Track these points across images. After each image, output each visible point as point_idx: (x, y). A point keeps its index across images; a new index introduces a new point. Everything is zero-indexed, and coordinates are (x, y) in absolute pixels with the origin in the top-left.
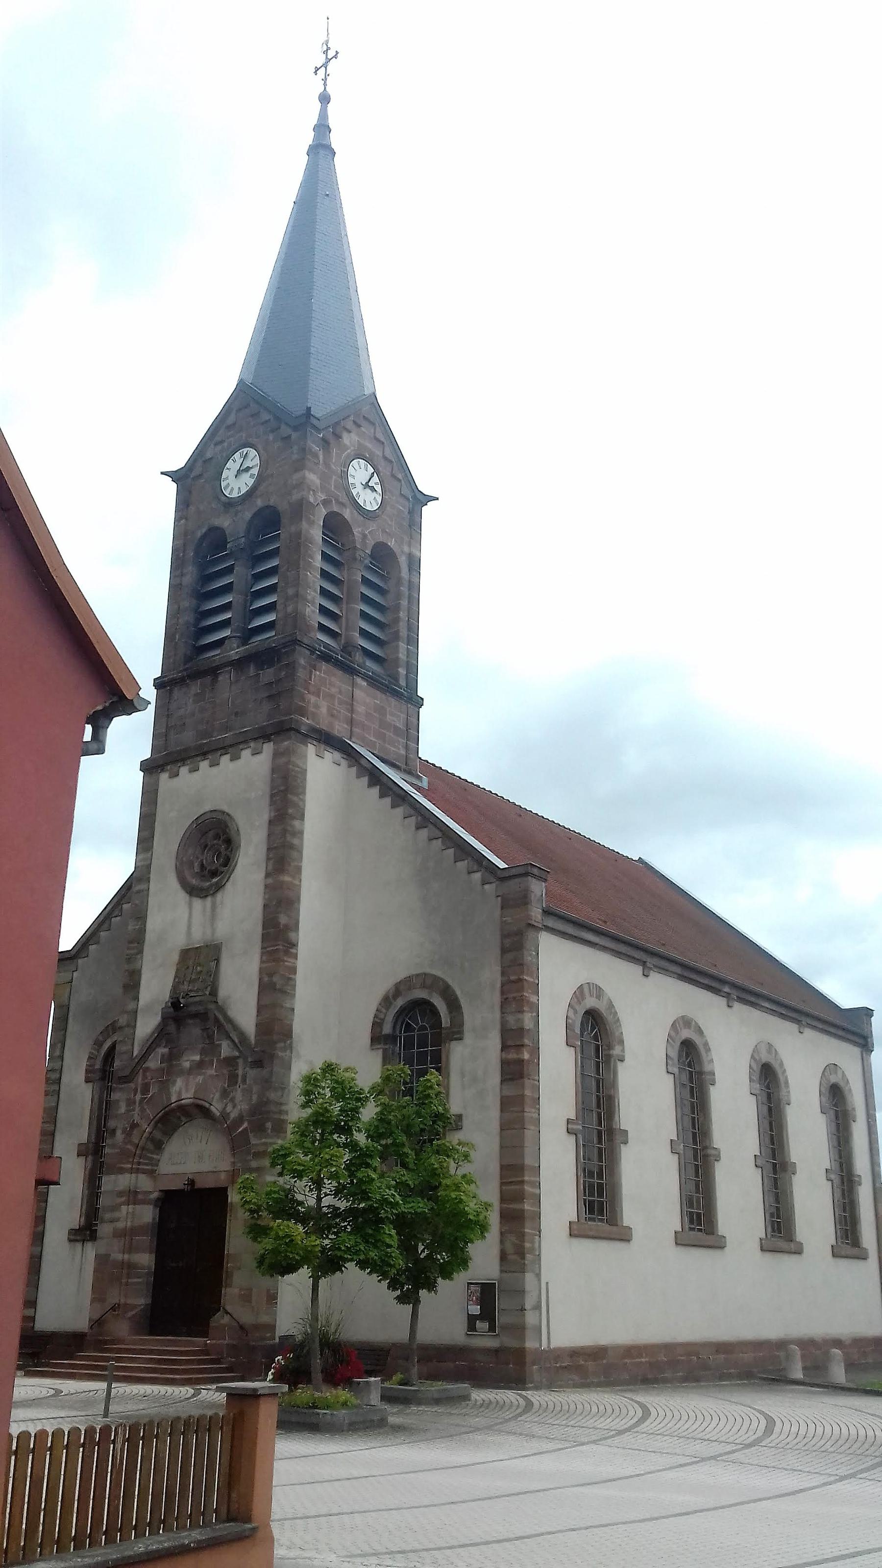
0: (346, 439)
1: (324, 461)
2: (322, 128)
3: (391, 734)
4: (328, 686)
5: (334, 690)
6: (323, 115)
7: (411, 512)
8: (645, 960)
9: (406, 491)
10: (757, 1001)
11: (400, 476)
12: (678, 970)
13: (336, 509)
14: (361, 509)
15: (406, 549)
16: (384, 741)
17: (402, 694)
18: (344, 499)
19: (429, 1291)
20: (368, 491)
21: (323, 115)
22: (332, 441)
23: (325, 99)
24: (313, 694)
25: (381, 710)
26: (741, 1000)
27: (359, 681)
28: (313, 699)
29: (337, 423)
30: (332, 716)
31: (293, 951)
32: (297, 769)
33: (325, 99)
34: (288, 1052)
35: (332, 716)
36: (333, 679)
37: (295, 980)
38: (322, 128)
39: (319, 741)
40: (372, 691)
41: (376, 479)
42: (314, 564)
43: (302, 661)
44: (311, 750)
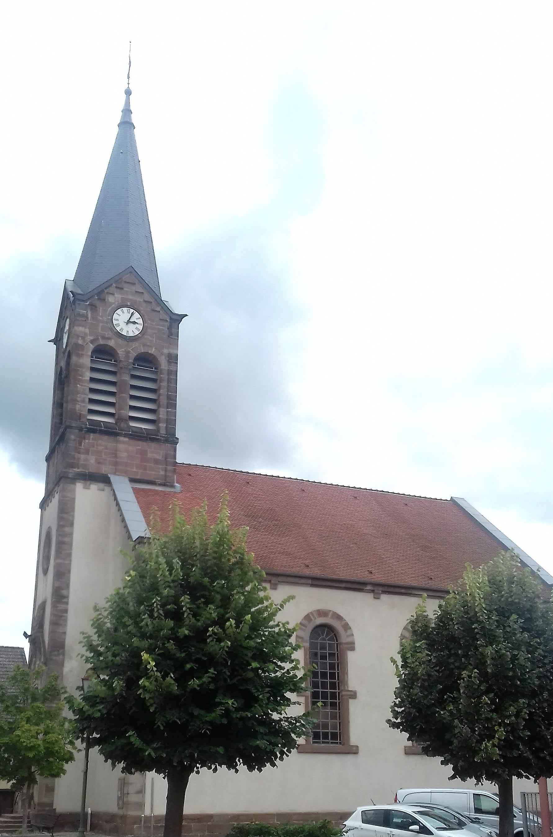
0: (111, 299)
1: (93, 318)
2: (127, 111)
3: (152, 465)
4: (95, 447)
5: (100, 448)
6: (128, 103)
7: (170, 328)
8: (270, 579)
9: (163, 316)
10: (410, 592)
11: (158, 309)
12: (310, 582)
13: (101, 342)
14: (122, 336)
15: (166, 351)
16: (146, 470)
17: (161, 440)
18: (108, 334)
19: (229, 768)
20: (131, 325)
21: (128, 103)
22: (98, 303)
23: (128, 93)
24: (83, 453)
25: (143, 453)
26: (384, 592)
27: (122, 439)
28: (82, 456)
29: (102, 291)
30: (99, 463)
31: (65, 600)
32: (66, 499)
33: (128, 93)
34: (61, 656)
35: (99, 463)
36: (100, 442)
37: (66, 617)
38: (127, 111)
39: (85, 480)
40: (133, 442)
41: (137, 315)
42: (84, 379)
43: (73, 437)
44: (79, 486)
